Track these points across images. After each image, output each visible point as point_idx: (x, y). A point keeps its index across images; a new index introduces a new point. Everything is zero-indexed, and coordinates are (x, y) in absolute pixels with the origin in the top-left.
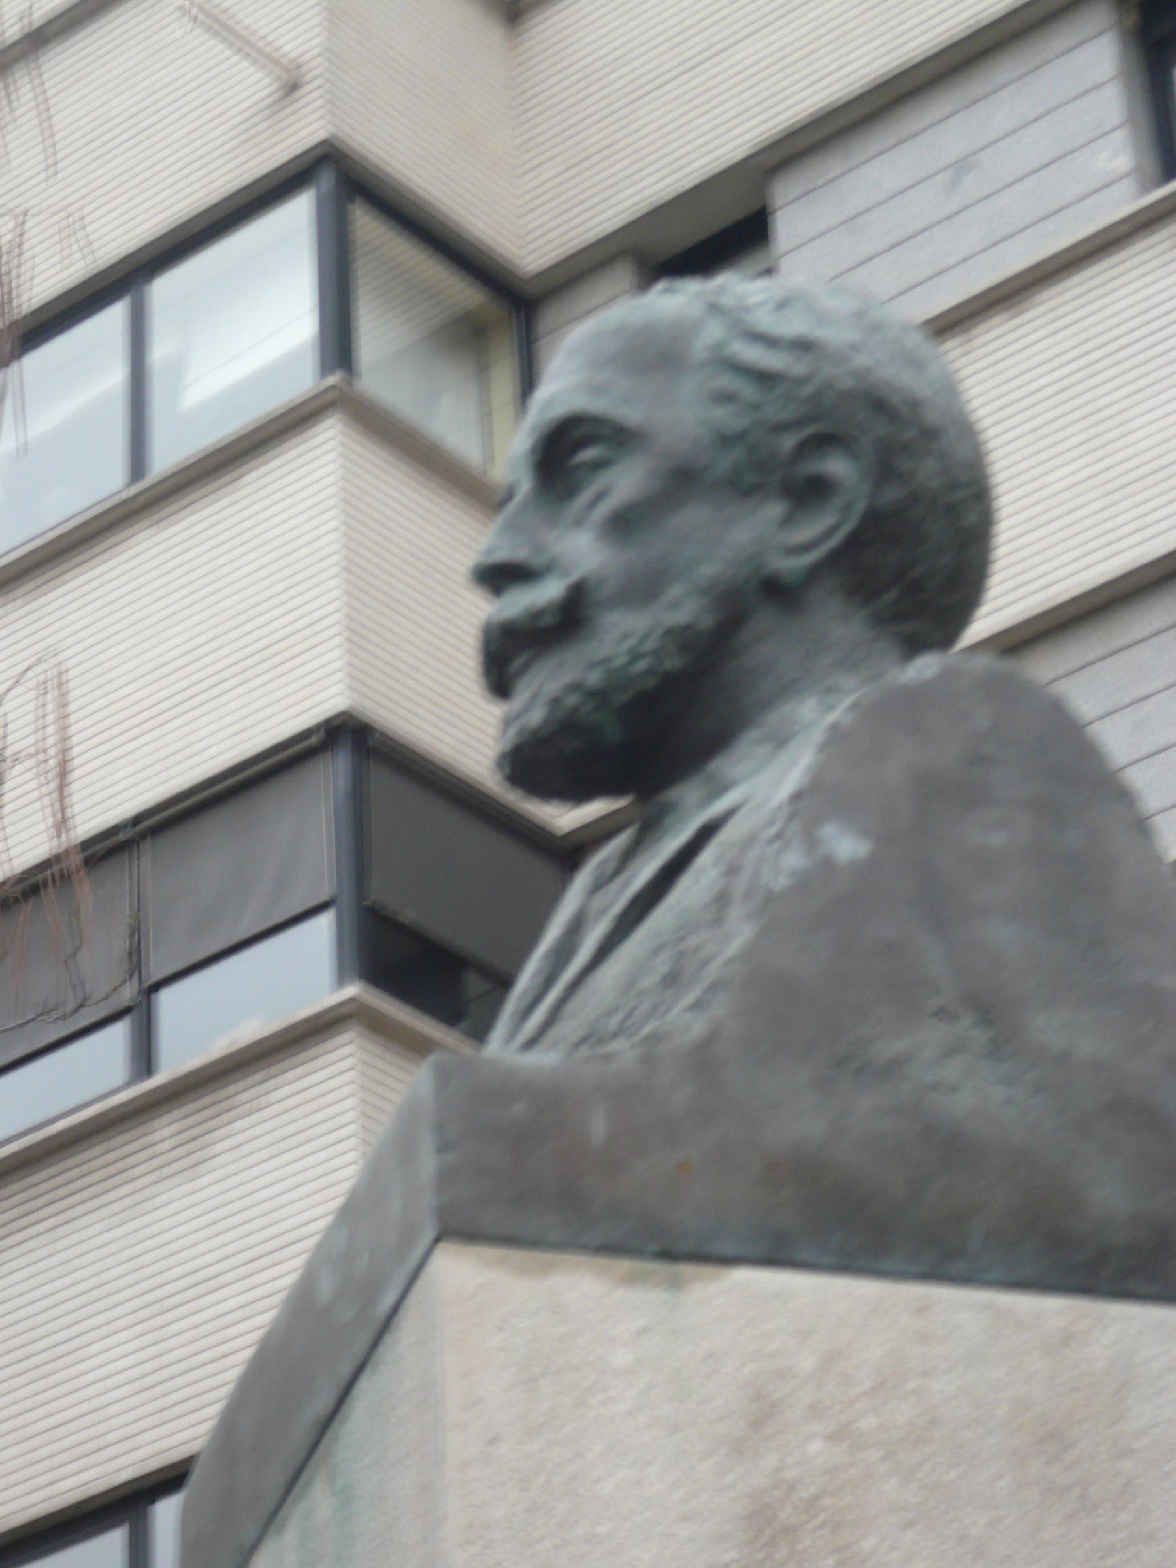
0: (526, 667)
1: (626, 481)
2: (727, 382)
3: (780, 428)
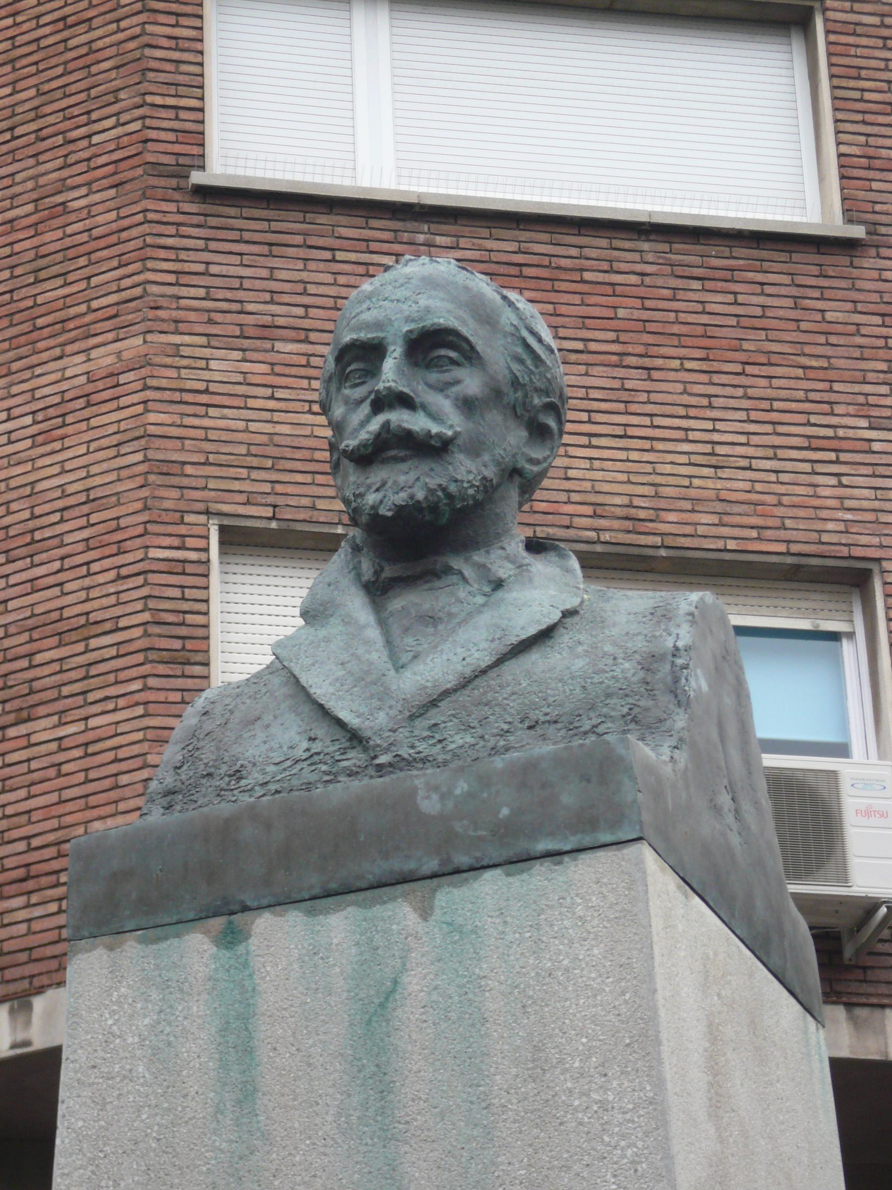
0: (403, 460)
1: (471, 383)
2: (520, 350)
3: (536, 390)
